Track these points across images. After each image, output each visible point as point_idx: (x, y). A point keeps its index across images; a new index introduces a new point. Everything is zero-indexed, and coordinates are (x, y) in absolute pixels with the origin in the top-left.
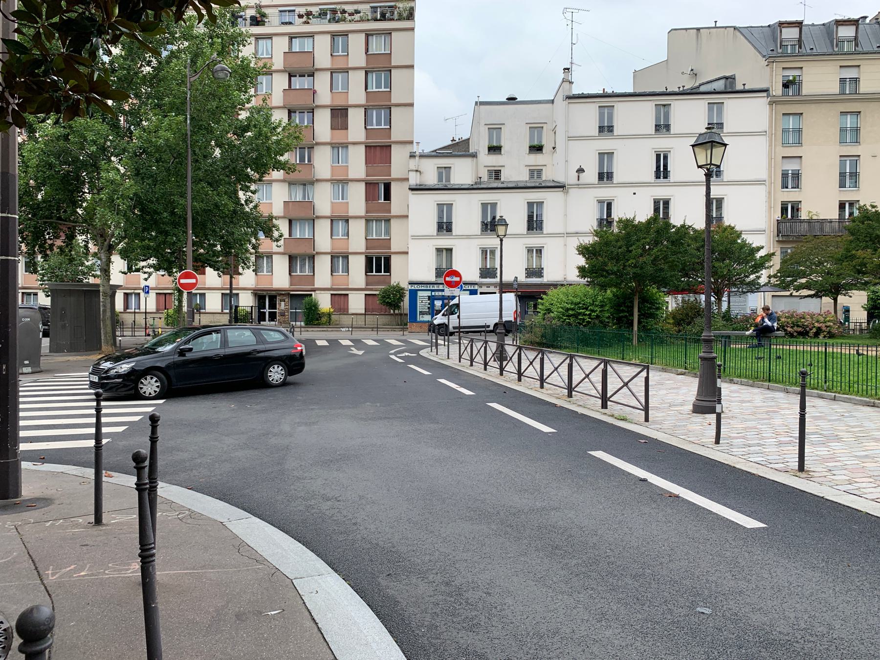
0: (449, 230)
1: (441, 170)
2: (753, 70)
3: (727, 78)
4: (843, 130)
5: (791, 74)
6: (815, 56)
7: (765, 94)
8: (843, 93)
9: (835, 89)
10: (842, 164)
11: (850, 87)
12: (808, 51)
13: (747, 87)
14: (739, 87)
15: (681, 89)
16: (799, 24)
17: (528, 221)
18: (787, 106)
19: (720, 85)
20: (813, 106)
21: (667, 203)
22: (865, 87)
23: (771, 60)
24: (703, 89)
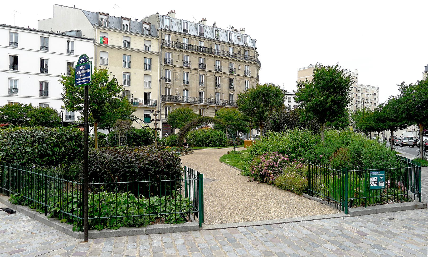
0: (47, 94)
1: (125, 74)
2: (88, 30)
3: (77, 31)
4: (124, 62)
5: (127, 39)
6: (113, 29)
7: (92, 41)
8: (124, 46)
9: (143, 48)
10: (124, 76)
11: (127, 44)
12: (111, 27)
13: (85, 37)
14: (82, 36)
15: (58, 32)
16: (107, 15)
17: (40, 91)
18: (126, 52)
19: (74, 34)
20: (112, 50)
21: (47, 84)
22: (133, 46)
23: (95, 27)
24: (67, 34)
